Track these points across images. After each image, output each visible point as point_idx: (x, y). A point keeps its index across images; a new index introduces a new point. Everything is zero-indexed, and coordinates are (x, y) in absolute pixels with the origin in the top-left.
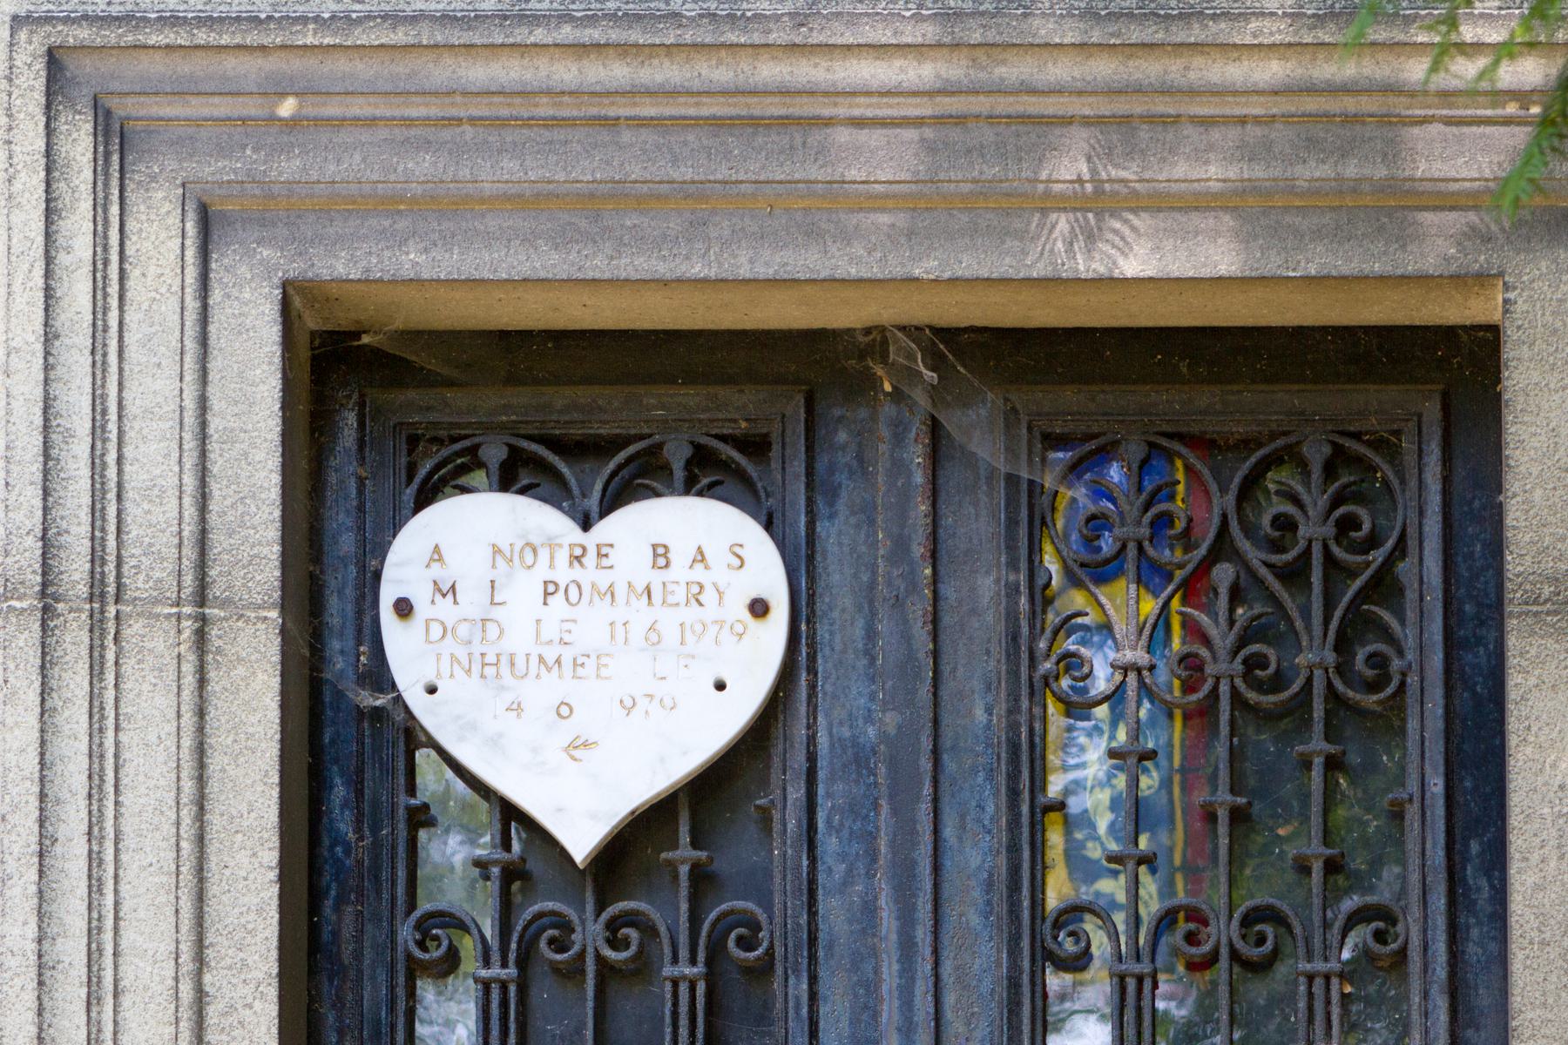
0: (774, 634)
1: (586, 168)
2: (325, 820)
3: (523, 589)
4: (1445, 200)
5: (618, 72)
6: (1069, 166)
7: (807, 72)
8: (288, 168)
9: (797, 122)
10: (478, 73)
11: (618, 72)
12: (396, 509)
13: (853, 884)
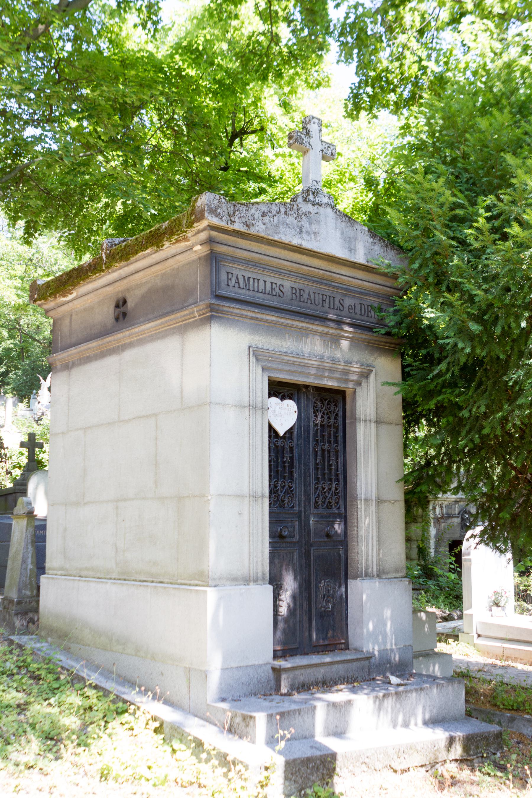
0: (296, 414)
1: (292, 368)
2: (123, 263)
3: (277, 407)
4: (352, 381)
5: (295, 359)
6: (327, 374)
7: (310, 362)
8: (269, 365)
9: (308, 366)
10: (285, 358)
11: (295, 359)
12: (300, 427)
13: (107, 238)
